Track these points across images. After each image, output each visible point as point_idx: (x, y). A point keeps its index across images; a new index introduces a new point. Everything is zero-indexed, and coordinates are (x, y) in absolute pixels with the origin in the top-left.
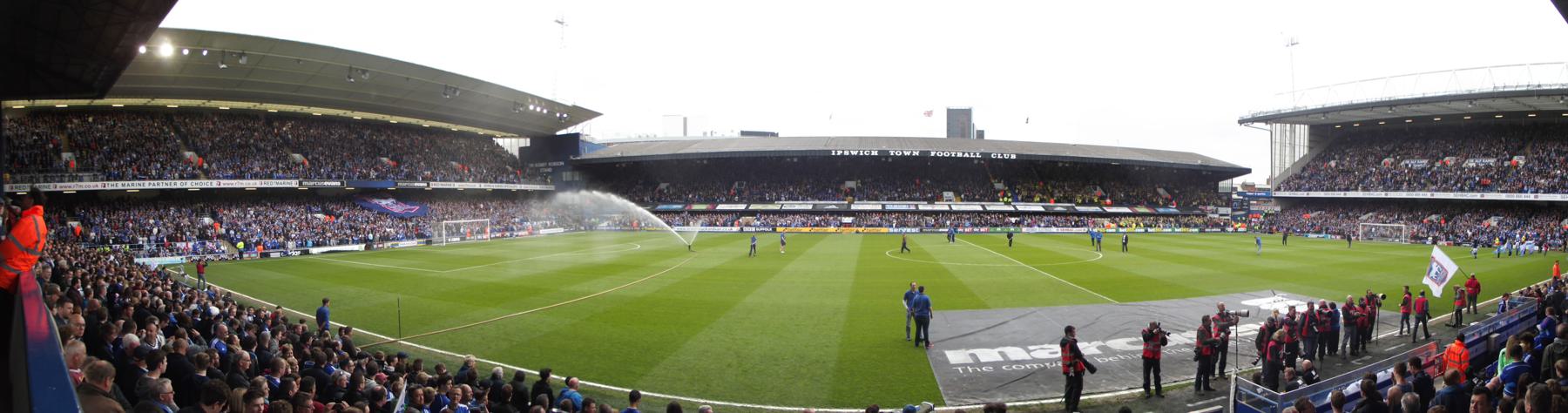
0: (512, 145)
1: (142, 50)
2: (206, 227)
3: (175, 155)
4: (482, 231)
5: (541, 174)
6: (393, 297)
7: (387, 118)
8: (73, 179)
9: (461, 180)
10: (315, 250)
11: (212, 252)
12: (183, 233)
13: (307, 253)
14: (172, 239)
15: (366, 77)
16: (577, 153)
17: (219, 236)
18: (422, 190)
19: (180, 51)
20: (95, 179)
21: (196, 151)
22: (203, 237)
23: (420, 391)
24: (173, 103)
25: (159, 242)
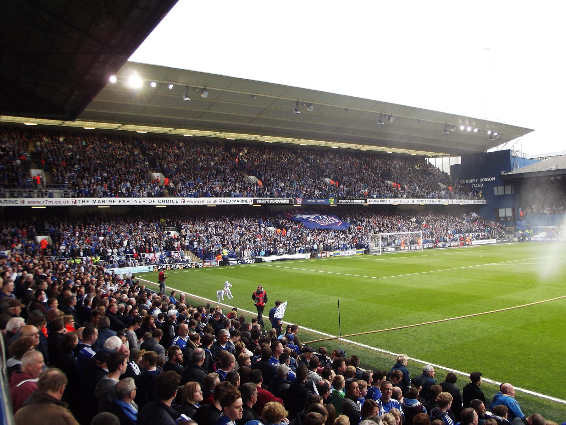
0: (443, 163)
1: (113, 79)
2: (172, 239)
3: (144, 176)
4: (414, 242)
5: (473, 190)
6: (334, 300)
7: (329, 144)
8: (42, 195)
9: (395, 197)
10: (267, 259)
11: (177, 261)
12: (150, 245)
13: (260, 261)
14: (141, 250)
15: (311, 109)
16: (509, 169)
17: (183, 247)
18: (360, 206)
19: (148, 84)
20: (66, 195)
21: (164, 172)
22: (169, 248)
23: (356, 384)
24: (142, 129)
25: (129, 254)
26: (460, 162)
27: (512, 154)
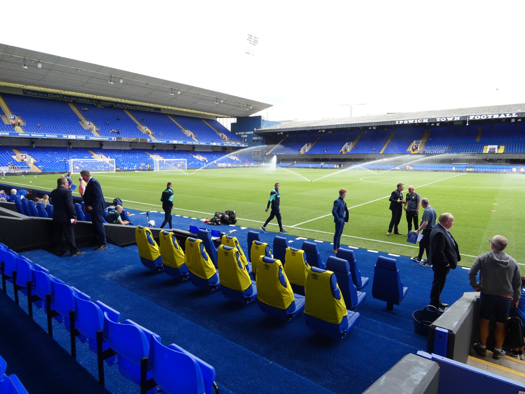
0: (227, 123)
26: (236, 122)
27: (262, 119)
